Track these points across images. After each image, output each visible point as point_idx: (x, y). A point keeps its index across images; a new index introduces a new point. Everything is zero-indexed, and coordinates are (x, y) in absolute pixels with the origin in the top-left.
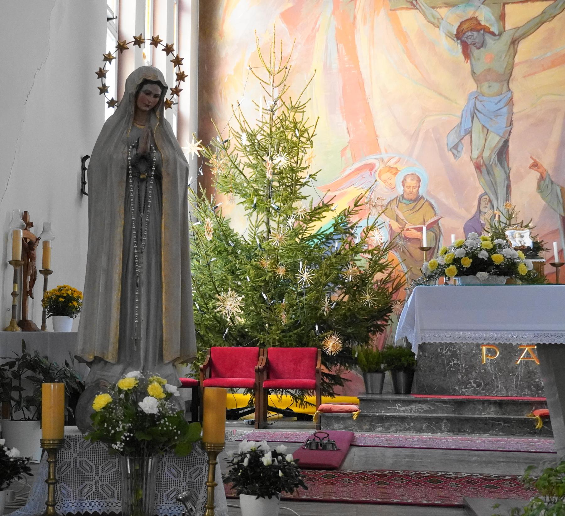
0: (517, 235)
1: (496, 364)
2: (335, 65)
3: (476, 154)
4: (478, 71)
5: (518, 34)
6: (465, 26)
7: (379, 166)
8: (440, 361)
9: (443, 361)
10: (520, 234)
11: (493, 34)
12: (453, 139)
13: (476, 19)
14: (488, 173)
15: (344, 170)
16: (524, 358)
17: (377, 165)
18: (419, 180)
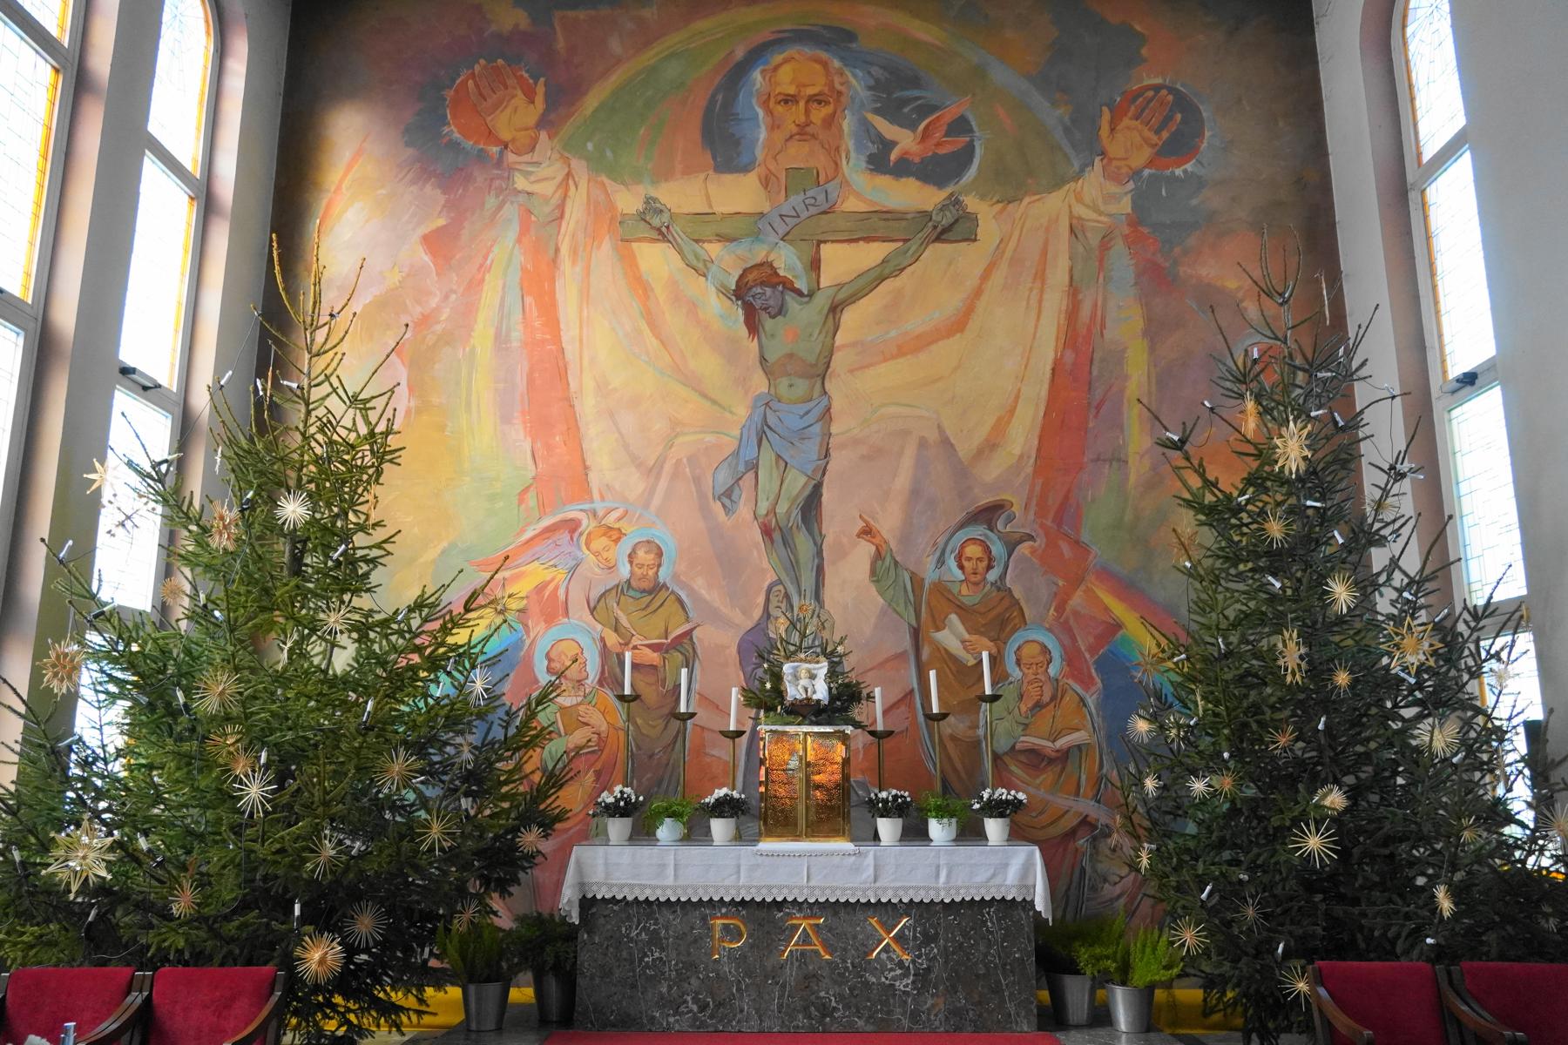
0: (803, 674)
1: (739, 959)
2: (517, 335)
3: (763, 507)
4: (772, 357)
5: (841, 296)
6: (751, 277)
7: (587, 524)
8: (625, 954)
9: (630, 954)
10: (809, 671)
11: (799, 293)
12: (724, 478)
13: (771, 265)
14: (785, 543)
15: (523, 531)
16: (797, 944)
17: (585, 522)
18: (660, 554)
